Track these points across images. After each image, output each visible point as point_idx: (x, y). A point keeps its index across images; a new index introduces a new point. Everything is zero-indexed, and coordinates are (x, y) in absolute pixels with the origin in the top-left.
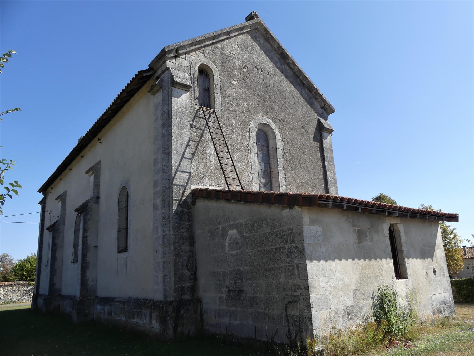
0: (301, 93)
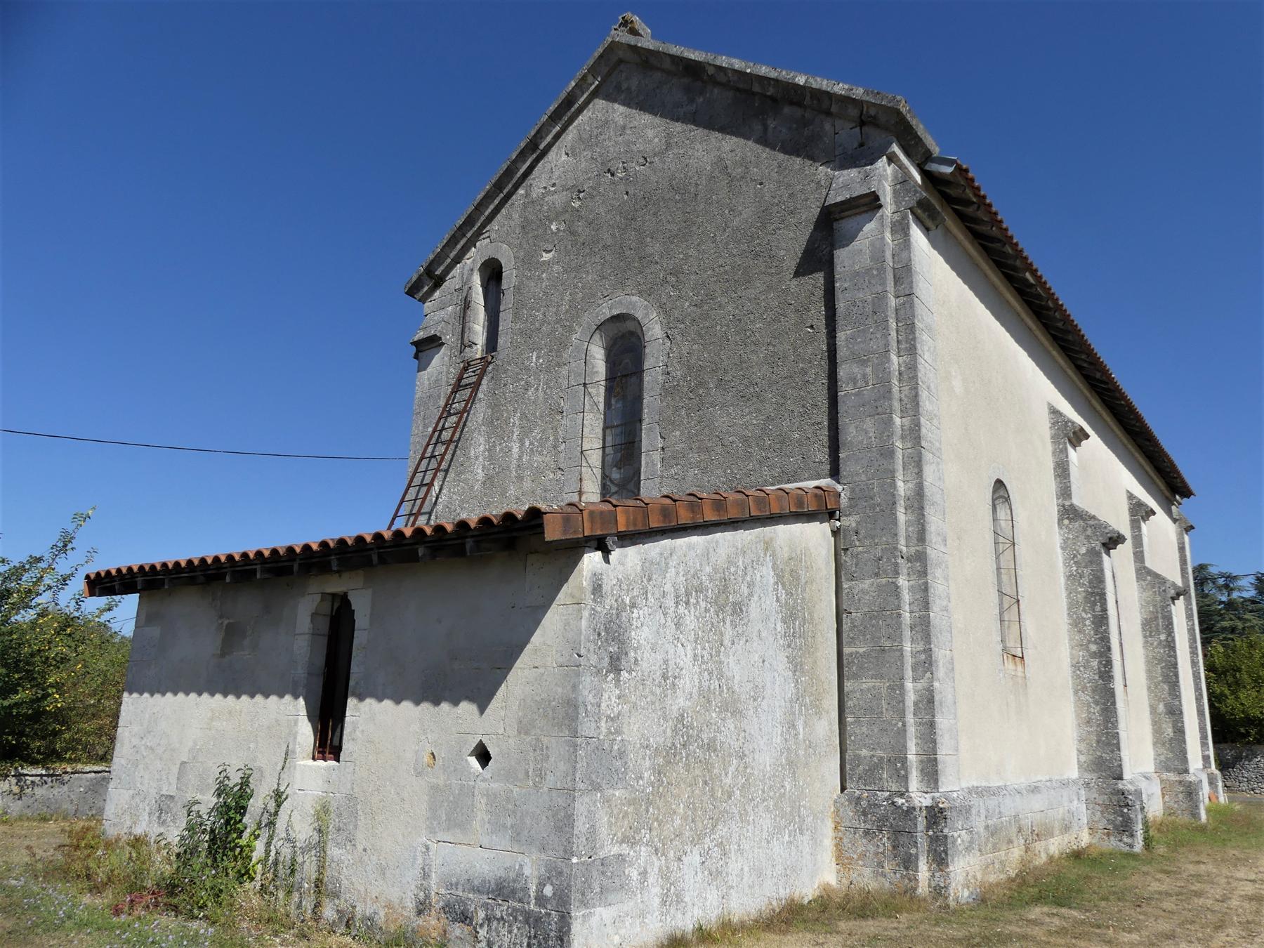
0: (764, 141)
